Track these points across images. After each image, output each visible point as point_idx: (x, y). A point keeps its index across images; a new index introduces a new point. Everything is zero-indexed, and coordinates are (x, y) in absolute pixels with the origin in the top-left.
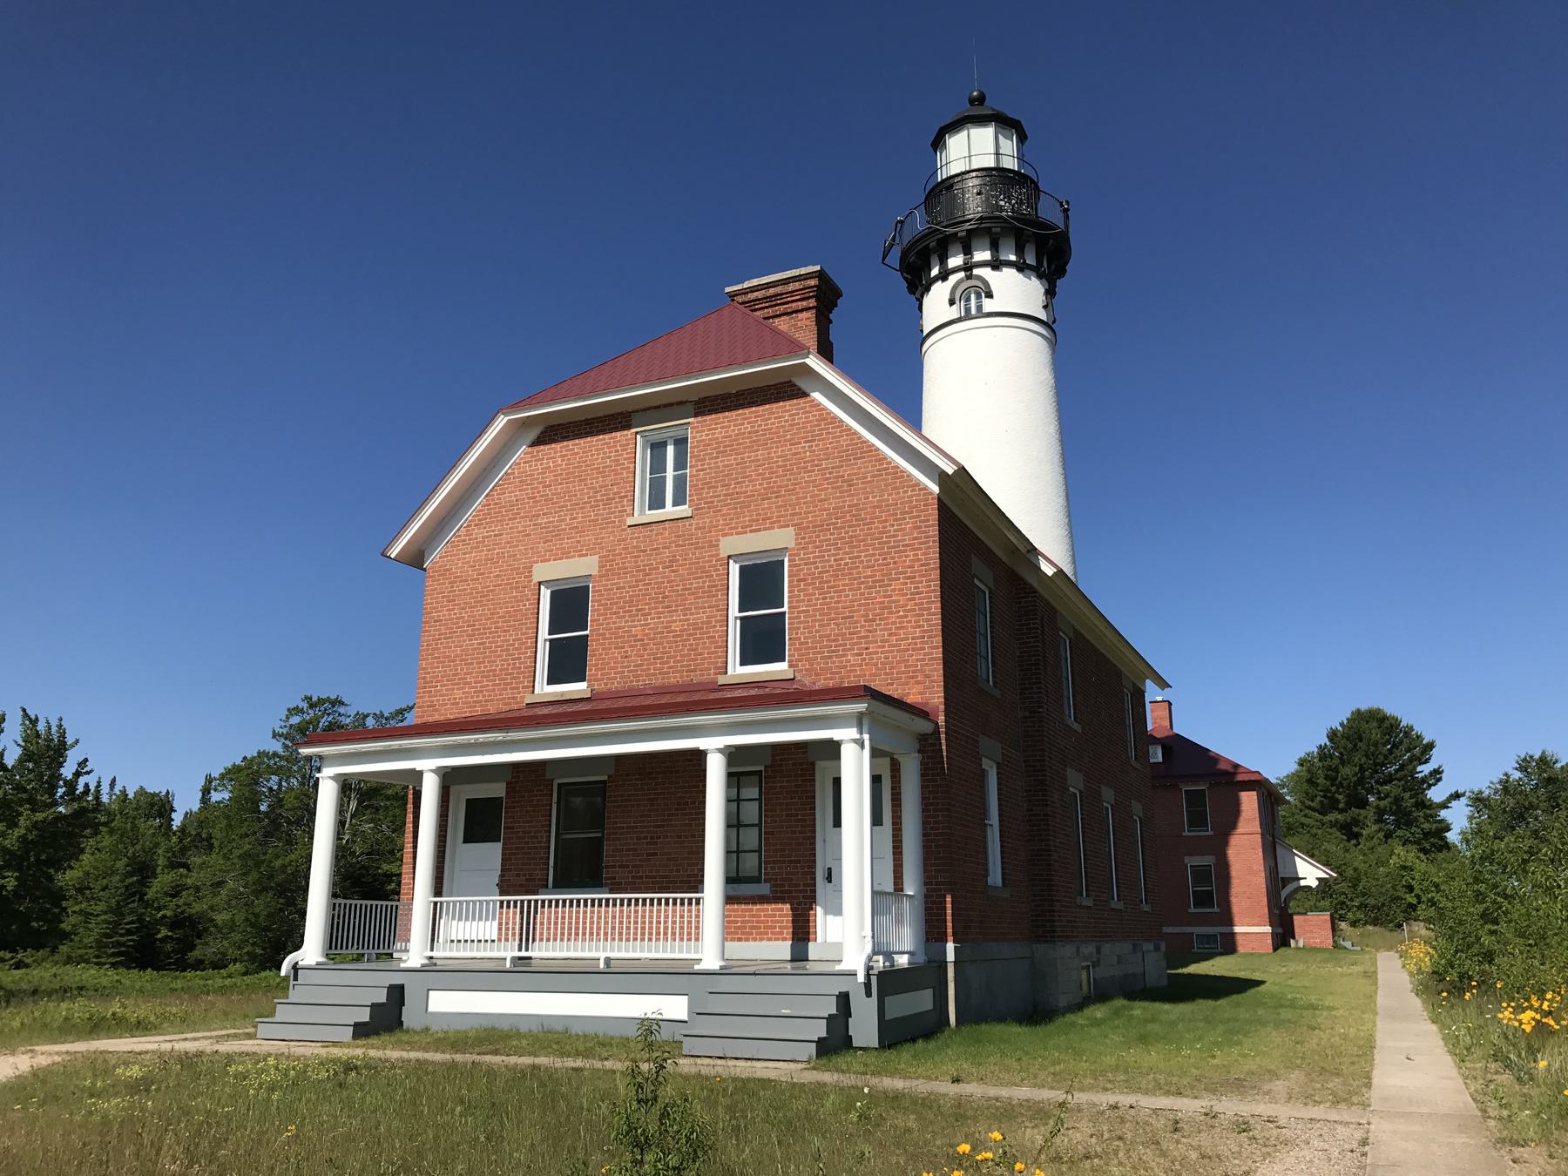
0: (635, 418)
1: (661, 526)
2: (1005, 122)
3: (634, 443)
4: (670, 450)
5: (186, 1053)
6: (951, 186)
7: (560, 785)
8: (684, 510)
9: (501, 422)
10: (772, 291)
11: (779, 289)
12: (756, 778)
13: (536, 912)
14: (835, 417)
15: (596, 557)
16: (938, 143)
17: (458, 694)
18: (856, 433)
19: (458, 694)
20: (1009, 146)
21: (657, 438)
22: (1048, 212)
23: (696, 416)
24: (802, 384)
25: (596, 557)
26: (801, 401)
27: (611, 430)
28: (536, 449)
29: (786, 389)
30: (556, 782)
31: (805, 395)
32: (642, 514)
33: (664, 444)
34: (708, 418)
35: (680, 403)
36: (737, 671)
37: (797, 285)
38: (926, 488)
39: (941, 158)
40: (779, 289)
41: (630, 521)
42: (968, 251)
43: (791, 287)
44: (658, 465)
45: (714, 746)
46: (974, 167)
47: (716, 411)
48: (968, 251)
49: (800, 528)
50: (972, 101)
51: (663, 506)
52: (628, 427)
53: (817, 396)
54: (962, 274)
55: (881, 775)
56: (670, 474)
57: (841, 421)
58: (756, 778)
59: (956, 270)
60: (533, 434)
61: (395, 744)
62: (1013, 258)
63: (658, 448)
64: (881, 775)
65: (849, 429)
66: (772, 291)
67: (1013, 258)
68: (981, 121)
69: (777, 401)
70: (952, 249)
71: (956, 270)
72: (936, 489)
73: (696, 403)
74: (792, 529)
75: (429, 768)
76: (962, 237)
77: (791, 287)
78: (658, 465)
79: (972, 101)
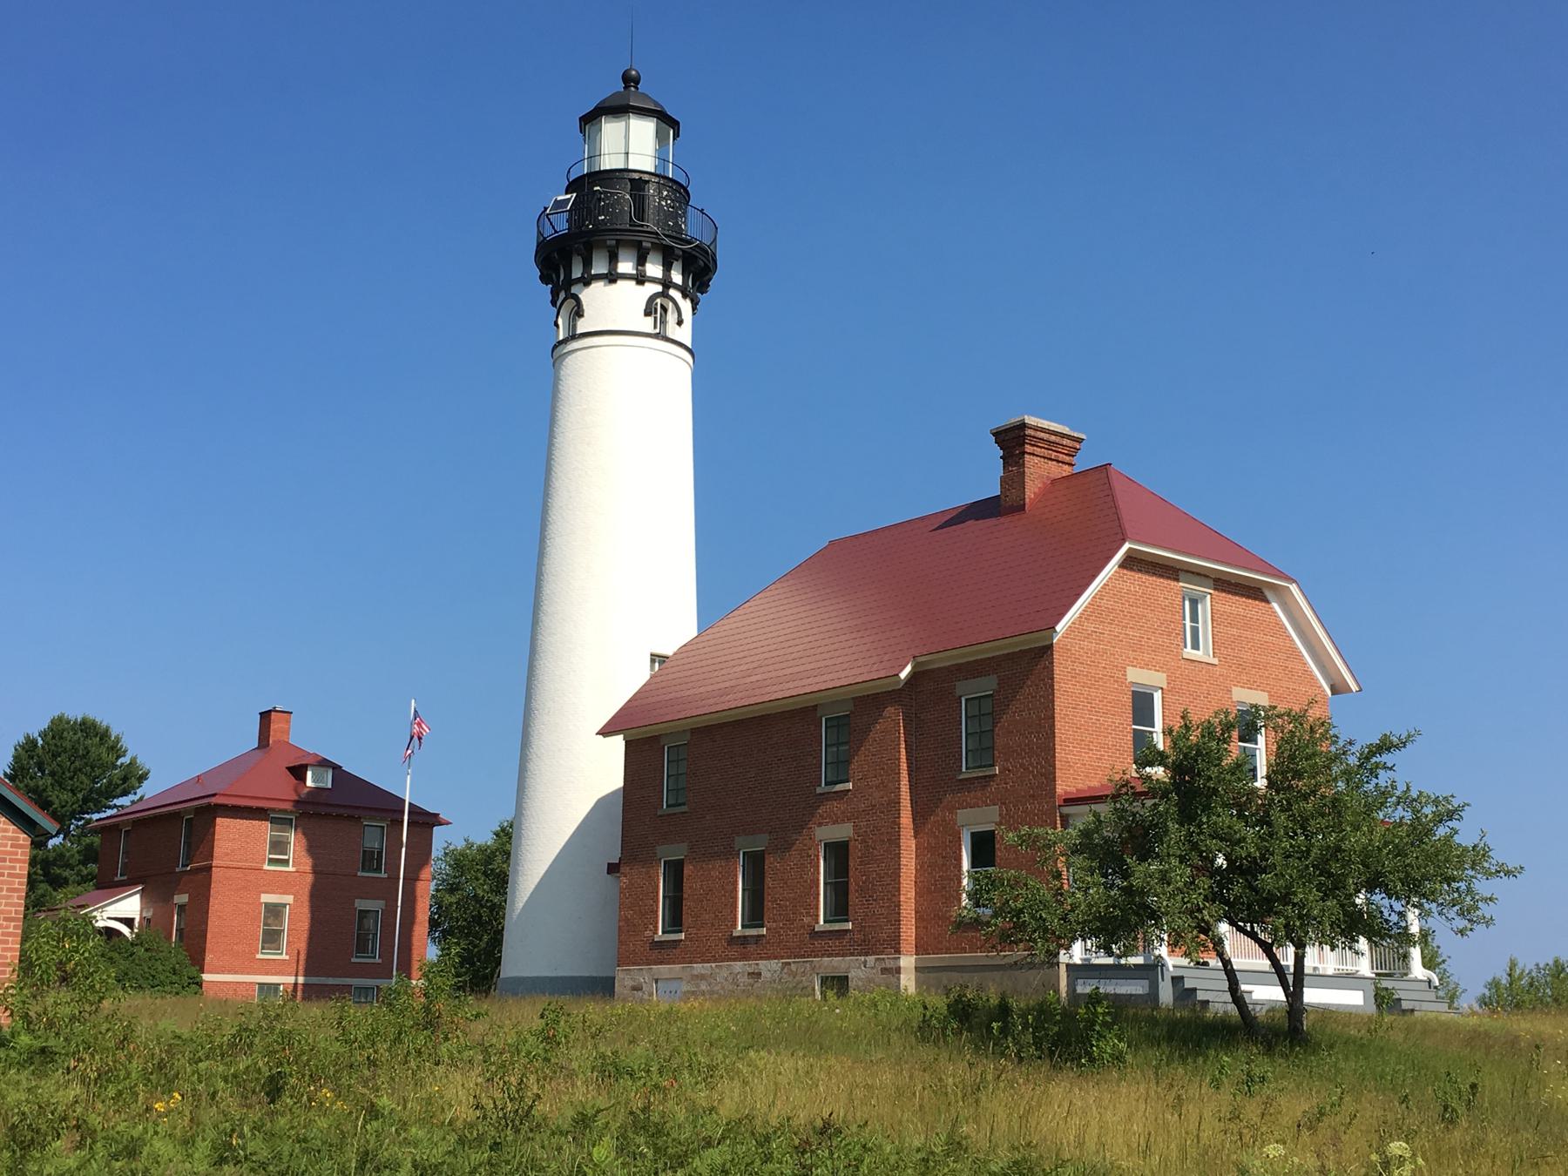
40: (1057, 439)
43: (1065, 442)
66: (1053, 438)
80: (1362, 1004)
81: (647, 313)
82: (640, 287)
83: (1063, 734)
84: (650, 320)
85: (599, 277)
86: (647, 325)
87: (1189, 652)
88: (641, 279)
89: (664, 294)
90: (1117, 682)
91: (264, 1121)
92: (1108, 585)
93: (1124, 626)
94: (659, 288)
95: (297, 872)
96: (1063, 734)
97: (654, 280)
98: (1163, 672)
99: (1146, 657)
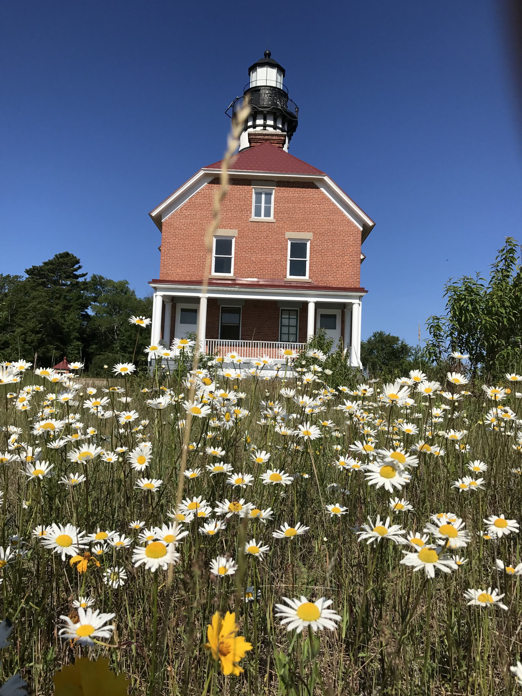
0: (253, 182)
1: (263, 224)
2: (281, 70)
3: (253, 190)
4: (263, 196)
5: (224, 377)
6: (259, 90)
7: (222, 307)
8: (271, 219)
9: (201, 173)
10: (266, 137)
11: (269, 137)
12: (296, 312)
13: (215, 348)
14: (328, 198)
15: (237, 231)
16: (253, 68)
17: (179, 271)
18: (335, 205)
19: (179, 271)
20: (280, 79)
21: (260, 191)
22: (291, 108)
23: (277, 186)
24: (318, 184)
25: (237, 231)
26: (317, 190)
27: (243, 185)
28: (211, 185)
29: (311, 185)
30: (221, 306)
31: (318, 188)
32: (254, 218)
33: (261, 194)
34: (282, 188)
35: (271, 181)
36: (289, 277)
37: (276, 138)
38: (358, 228)
39: (253, 76)
40: (269, 137)
41: (250, 220)
42: (265, 120)
43: (274, 138)
44: (258, 201)
45: (312, 301)
46: (268, 85)
47: (285, 187)
48: (265, 120)
49: (314, 233)
50: (266, 55)
51: (260, 216)
52: (250, 185)
53: (322, 189)
54: (262, 128)
55: (336, 315)
56: (263, 205)
57: (330, 200)
58: (296, 312)
59: (259, 126)
60: (210, 179)
61: (193, 287)
62: (281, 126)
63: (259, 194)
64: (336, 315)
65: (333, 203)
66: (266, 137)
67: (281, 126)
68: (272, 65)
69: (308, 188)
70: (258, 116)
71: (259, 126)
72: (361, 229)
73: (277, 182)
74: (312, 233)
75: (312, 301)
76: (265, 113)
77: (274, 138)
78: (258, 201)
79: (266, 55)
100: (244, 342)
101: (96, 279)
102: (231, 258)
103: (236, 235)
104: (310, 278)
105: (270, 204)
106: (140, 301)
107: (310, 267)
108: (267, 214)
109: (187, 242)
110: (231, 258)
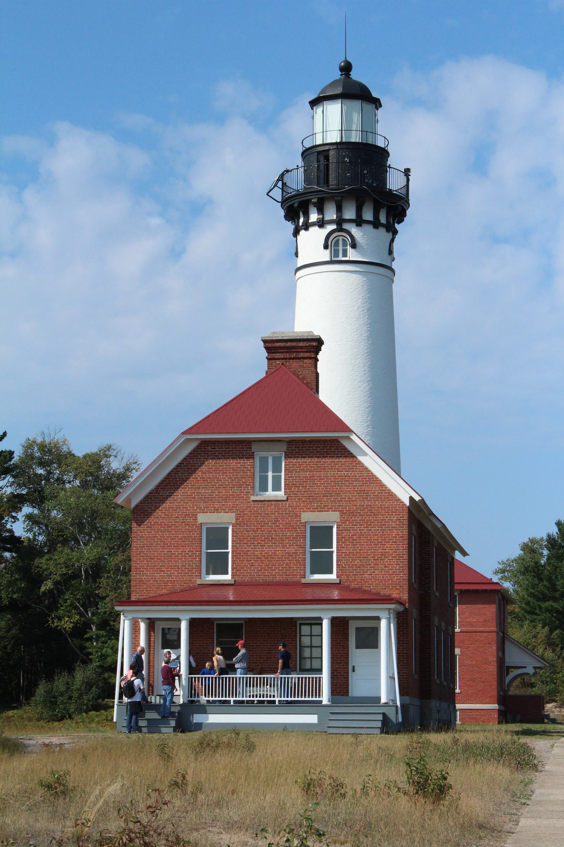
8: (281, 494)
11: (294, 344)
15: (234, 514)
25: (234, 514)
40: (294, 344)
43: (301, 344)
46: (329, 141)
49: (342, 513)
66: (289, 344)
77: (301, 344)
80: (317, 716)
81: (326, 247)
82: (308, 232)
83: (138, 564)
84: (328, 252)
85: (313, 224)
86: (326, 255)
87: (271, 494)
88: (321, 224)
89: (340, 229)
90: (188, 525)
91: (360, 796)
92: (183, 464)
93: (197, 488)
94: (334, 227)
95: (461, 632)
96: (138, 564)
97: (331, 222)
98: (233, 512)
99: (217, 505)
100: (299, 678)
101: (174, 671)
102: (228, 553)
103: (234, 521)
104: (337, 577)
105: (114, 699)
106: (16, 537)
107: (337, 561)
108: (277, 488)
109: (166, 535)
110: (228, 553)
